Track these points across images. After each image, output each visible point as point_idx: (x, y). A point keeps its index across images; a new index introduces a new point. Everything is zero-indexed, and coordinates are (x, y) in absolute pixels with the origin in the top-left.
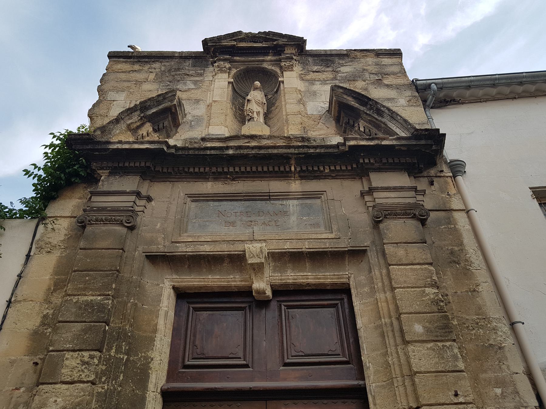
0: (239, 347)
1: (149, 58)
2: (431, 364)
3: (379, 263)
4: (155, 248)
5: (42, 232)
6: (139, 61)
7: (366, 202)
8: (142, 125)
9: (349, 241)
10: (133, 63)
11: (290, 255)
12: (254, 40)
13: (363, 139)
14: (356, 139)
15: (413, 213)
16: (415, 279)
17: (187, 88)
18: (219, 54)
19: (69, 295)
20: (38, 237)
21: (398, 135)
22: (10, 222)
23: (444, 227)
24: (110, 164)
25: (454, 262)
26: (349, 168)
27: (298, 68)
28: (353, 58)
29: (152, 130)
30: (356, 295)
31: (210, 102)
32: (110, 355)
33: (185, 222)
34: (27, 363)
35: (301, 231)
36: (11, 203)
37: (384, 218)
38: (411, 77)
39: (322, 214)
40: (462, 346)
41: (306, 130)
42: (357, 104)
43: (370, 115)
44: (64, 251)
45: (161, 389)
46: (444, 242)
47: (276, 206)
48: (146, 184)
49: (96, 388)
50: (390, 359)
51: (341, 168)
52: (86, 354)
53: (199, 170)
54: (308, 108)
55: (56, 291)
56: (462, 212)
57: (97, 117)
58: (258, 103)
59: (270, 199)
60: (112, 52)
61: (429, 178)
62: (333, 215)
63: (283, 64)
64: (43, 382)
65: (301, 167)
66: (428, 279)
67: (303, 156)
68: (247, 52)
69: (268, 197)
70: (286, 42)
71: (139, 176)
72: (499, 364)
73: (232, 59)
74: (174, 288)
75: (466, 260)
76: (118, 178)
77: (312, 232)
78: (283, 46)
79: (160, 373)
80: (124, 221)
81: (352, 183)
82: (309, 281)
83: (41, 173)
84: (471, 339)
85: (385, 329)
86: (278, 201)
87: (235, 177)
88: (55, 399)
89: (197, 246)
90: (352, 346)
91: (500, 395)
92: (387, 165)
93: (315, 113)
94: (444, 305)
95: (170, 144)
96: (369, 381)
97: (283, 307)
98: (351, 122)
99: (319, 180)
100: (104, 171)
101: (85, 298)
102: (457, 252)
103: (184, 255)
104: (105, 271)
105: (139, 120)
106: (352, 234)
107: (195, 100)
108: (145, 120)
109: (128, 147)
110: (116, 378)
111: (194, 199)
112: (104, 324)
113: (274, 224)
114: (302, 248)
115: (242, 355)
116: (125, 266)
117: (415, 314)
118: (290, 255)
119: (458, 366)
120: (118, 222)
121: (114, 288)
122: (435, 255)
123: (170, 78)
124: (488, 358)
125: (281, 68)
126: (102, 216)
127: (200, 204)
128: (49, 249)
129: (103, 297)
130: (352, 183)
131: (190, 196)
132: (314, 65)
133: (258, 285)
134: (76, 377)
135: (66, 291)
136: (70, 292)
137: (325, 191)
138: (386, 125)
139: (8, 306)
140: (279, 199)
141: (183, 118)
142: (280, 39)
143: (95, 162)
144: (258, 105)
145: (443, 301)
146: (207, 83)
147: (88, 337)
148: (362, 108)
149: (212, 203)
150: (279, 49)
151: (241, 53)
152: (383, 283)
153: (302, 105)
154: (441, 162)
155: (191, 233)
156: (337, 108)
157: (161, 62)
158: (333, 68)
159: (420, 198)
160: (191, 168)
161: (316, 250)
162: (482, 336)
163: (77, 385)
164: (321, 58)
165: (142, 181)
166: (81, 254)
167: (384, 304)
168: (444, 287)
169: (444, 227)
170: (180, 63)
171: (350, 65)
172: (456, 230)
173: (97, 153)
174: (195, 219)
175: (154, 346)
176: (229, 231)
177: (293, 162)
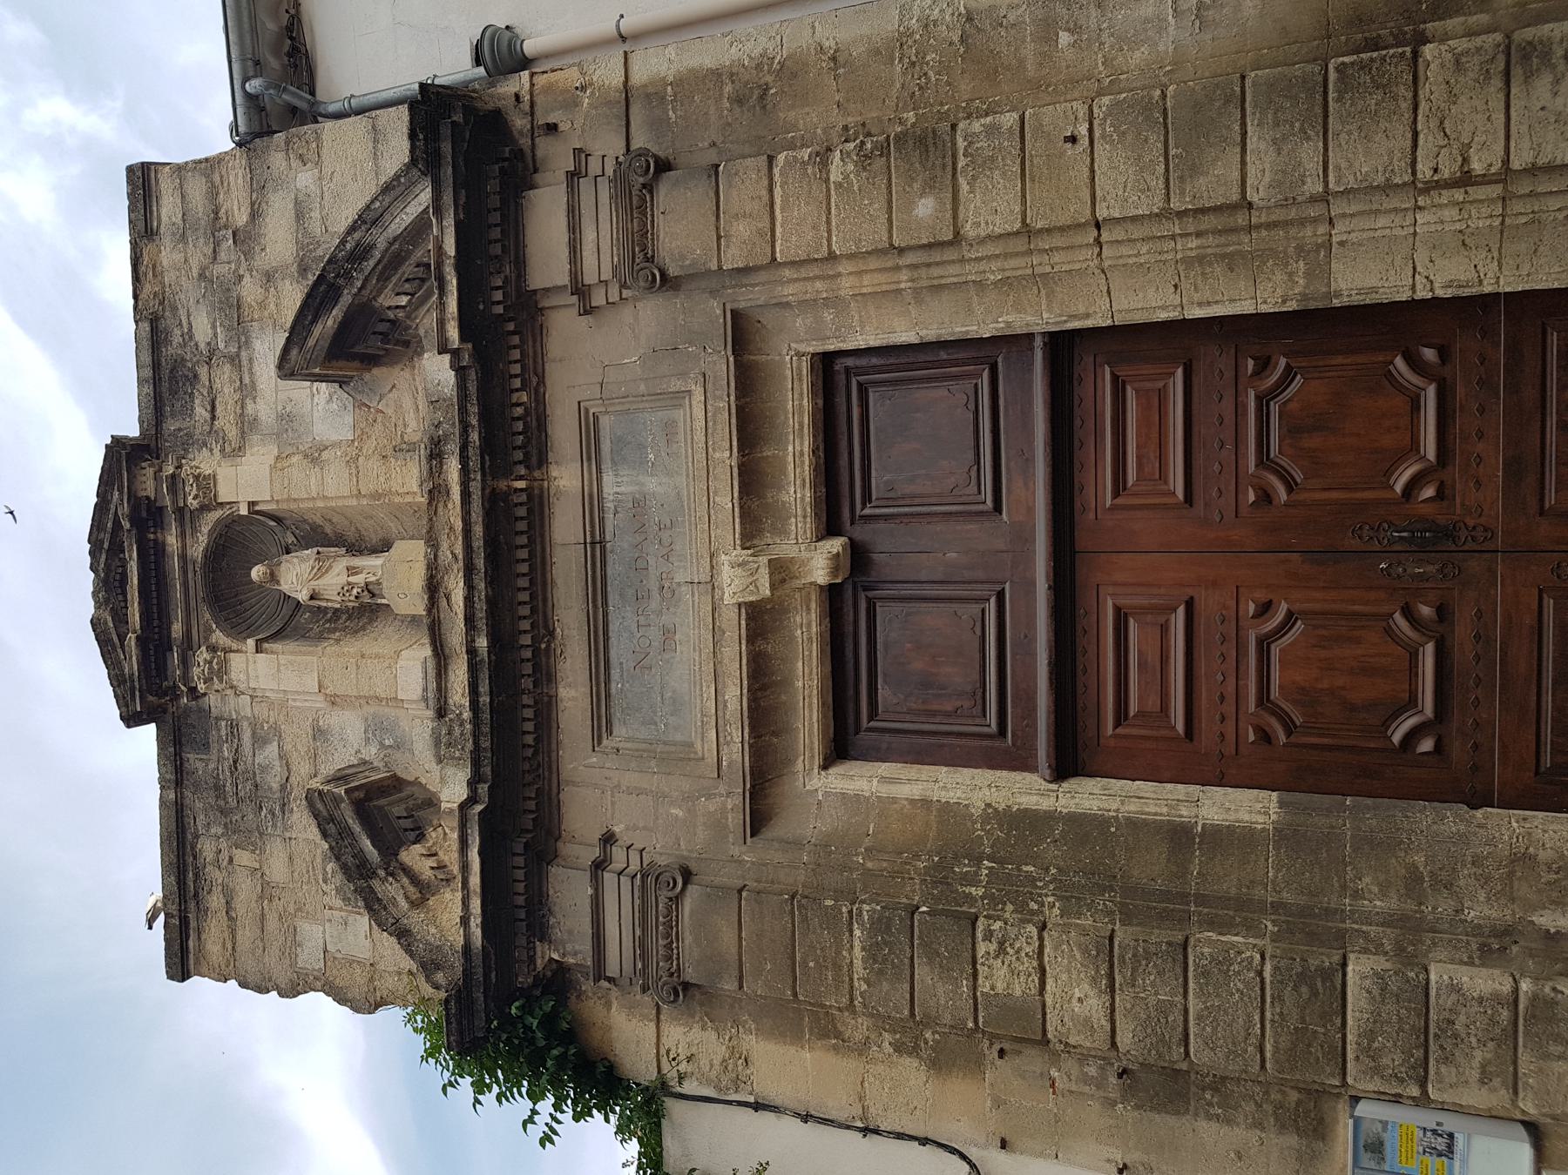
0: (959, 614)
1: (185, 871)
2: (1005, 187)
3: (769, 282)
4: (733, 817)
5: (696, 1083)
6: (196, 895)
7: (608, 303)
8: (407, 871)
9: (710, 351)
10: (202, 911)
11: (748, 495)
12: (117, 584)
13: (442, 305)
14: (442, 323)
15: (641, 191)
16: (807, 204)
17: (277, 763)
18: (166, 679)
19: (852, 1000)
20: (709, 1092)
21: (428, 207)
22: (671, 1161)
23: (671, 113)
24: (522, 941)
25: (762, 97)
26: (516, 340)
27: (204, 462)
28: (162, 303)
29: (418, 846)
30: (842, 341)
31: (322, 698)
32: (983, 898)
33: (667, 748)
34: (999, 1072)
35: (685, 467)
36: (624, 1165)
37: (653, 262)
38: (223, 143)
39: (641, 415)
40: (965, 108)
41: (404, 446)
42: (334, 312)
43: (366, 280)
44: (744, 1027)
45: (1050, 782)
46: (713, 118)
47: (621, 526)
48: (566, 849)
49: (1053, 920)
50: (992, 277)
51: (516, 362)
52: (982, 948)
53: (529, 720)
54: (335, 437)
55: (841, 1033)
56: (630, 61)
57: (375, 989)
58: (321, 573)
59: (602, 542)
60: (167, 972)
61: (536, 134)
62: (642, 387)
63: (195, 503)
64: (1040, 1032)
65: (515, 463)
66: (809, 171)
67: (487, 458)
68: (155, 601)
69: (596, 546)
70: (121, 493)
71: (550, 867)
72: (1006, 28)
73: (183, 643)
74: (825, 767)
75: (759, 67)
76: (555, 917)
77: (689, 441)
78: (136, 502)
79: (1018, 786)
80: (670, 894)
81: (554, 333)
82: (806, 450)
83: (546, 1106)
84: (948, 83)
85: (925, 283)
86: (607, 521)
87: (545, 629)
88: (1074, 1001)
89: (727, 717)
90: (956, 356)
91: (1073, 35)
92: (507, 243)
93: (349, 419)
94: (872, 141)
95: (465, 796)
96: (1038, 324)
97: (867, 511)
98: (382, 327)
99: (548, 419)
100: (539, 954)
101: (858, 963)
102: (737, 88)
103: (751, 746)
104: (794, 926)
105: (396, 880)
106: (691, 344)
107: (314, 739)
108: (393, 864)
109: (479, 902)
110: (1032, 880)
111: (604, 729)
112: (916, 917)
113: (669, 532)
114: (731, 466)
115: (977, 606)
116: (779, 883)
117: (891, 212)
118: (748, 495)
119: (1011, 127)
120: (674, 907)
121: (833, 902)
122: (747, 145)
123: (248, 809)
124: (992, 51)
125: (204, 508)
126: (658, 945)
127: (617, 715)
128: (741, 1061)
129: (855, 923)
130: (554, 333)
131: (597, 739)
132: (190, 415)
133: (821, 572)
134: (1029, 965)
135: (840, 1009)
136: (845, 1000)
137: (579, 403)
138: (395, 239)
139: (876, 1132)
140: (602, 520)
141: (374, 769)
142: (112, 511)
143: (517, 979)
144: (327, 571)
145: (863, 143)
146: (261, 711)
147: (946, 947)
148: (346, 299)
149: (613, 685)
150: (144, 514)
151: (160, 619)
152: (817, 277)
153: (325, 455)
154: (492, 96)
155: (693, 734)
156: (341, 363)
157: (197, 836)
158: (198, 362)
159: (594, 166)
160: (525, 742)
161: (734, 433)
162: (941, 57)
163: (1046, 959)
164: (166, 395)
165: (559, 860)
166: (757, 987)
167: (867, 279)
168: (825, 130)
169: (671, 113)
170: (196, 785)
171: (189, 316)
172: (679, 82)
173: (493, 975)
174: (656, 724)
175: (959, 804)
176: (689, 641)
177: (502, 485)
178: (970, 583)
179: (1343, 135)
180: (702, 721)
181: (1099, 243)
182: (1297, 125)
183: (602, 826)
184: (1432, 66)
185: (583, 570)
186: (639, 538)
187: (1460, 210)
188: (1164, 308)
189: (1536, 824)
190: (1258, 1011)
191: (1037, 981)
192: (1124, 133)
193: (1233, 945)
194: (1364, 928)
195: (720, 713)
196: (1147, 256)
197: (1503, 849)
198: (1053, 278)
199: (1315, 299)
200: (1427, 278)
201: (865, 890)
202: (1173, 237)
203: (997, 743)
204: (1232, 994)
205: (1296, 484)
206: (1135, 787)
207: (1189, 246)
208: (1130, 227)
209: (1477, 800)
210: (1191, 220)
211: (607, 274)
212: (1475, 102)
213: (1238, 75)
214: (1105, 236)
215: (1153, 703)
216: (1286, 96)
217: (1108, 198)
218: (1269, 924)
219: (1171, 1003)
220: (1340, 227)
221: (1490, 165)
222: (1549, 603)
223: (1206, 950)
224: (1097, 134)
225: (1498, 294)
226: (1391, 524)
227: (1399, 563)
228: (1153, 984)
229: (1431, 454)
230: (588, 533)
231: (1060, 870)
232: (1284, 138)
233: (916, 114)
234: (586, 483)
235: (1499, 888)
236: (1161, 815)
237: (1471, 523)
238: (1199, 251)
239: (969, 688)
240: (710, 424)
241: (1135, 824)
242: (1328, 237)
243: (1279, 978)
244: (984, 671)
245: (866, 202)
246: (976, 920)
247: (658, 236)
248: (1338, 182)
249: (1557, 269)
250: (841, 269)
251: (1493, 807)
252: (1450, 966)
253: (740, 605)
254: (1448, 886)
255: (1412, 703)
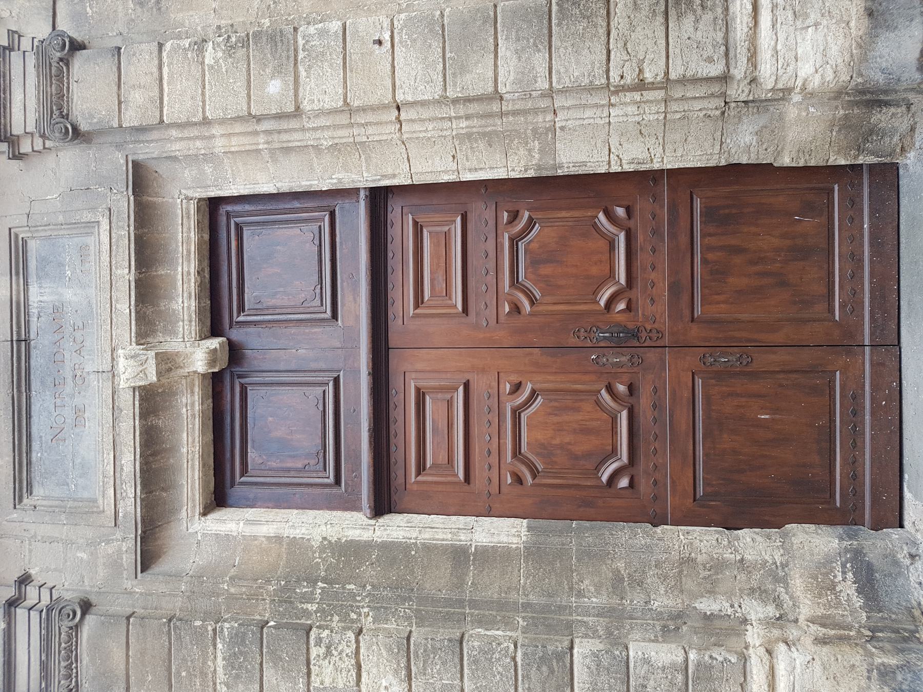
0: (307, 394)
7: (33, 151)
9: (115, 191)
15: (58, 63)
16: (187, 80)
23: (88, 9)
30: (220, 189)
32: (316, 612)
33: (76, 504)
37: (67, 119)
39: (61, 240)
40: (305, 18)
45: (370, 519)
46: (120, 15)
50: (325, 143)
52: (314, 652)
66: (189, 56)
74: (204, 514)
79: (347, 522)
80: (71, 624)
82: (192, 271)
85: (277, 145)
89: (123, 477)
90: (306, 205)
94: (236, 36)
96: (360, 181)
97: (241, 319)
101: (220, 671)
103: (142, 500)
104: (170, 643)
110: (353, 595)
111: (25, 490)
112: (265, 630)
114: (129, 281)
115: (321, 388)
118: (143, 303)
119: (336, 32)
120: (74, 634)
129: (218, 639)
131: (18, 498)
133: (200, 363)
137: (10, 229)
140: (27, 323)
145: (229, 37)
147: (287, 654)
149: (34, 455)
152: (197, 138)
155: (97, 491)
161: (133, 255)
163: (362, 657)
167: (234, 141)
168: (203, 28)
169: (88, 9)
174: (68, 484)
175: (303, 538)
178: (315, 371)
179: (562, 49)
180: (103, 482)
181: (400, 121)
182: (531, 40)
183: (21, 570)
184: (619, 5)
185: (10, 362)
186: (57, 337)
187: (638, 107)
188: (446, 172)
189: (695, 536)
190: (513, 687)
191: (354, 675)
192: (415, 40)
193: (495, 638)
194: (585, 619)
195: (118, 475)
196: (433, 132)
197: (675, 556)
198: (369, 146)
199: (546, 169)
200: (618, 156)
201: (227, 611)
202: (450, 119)
203: (335, 490)
204: (495, 676)
205: (536, 300)
206: (430, 520)
207: (461, 125)
208: (420, 109)
209: (657, 521)
210: (461, 106)
211: (31, 128)
212: (647, 32)
213: (492, 4)
214: (403, 116)
215: (443, 458)
216: (524, 20)
217: (404, 86)
218: (520, 620)
219: (452, 686)
220: (561, 115)
221: (657, 75)
222: (699, 382)
223: (476, 644)
224: (396, 40)
225: (663, 170)
226: (598, 328)
227: (604, 355)
228: (439, 673)
229: (623, 281)
230: (15, 333)
231: (373, 586)
232: (523, 49)
233: (271, 20)
234: (14, 293)
235: (673, 584)
236: (447, 540)
237: (649, 327)
238: (468, 130)
239: (314, 451)
240: (114, 248)
241: (428, 548)
242: (553, 123)
243: (527, 661)
244: (325, 436)
245: (231, 81)
246: (310, 630)
247: (72, 99)
248: (558, 82)
249: (700, 153)
250: (214, 131)
251: (668, 525)
252: (643, 644)
253: (134, 389)
254: (640, 584)
255: (613, 452)
